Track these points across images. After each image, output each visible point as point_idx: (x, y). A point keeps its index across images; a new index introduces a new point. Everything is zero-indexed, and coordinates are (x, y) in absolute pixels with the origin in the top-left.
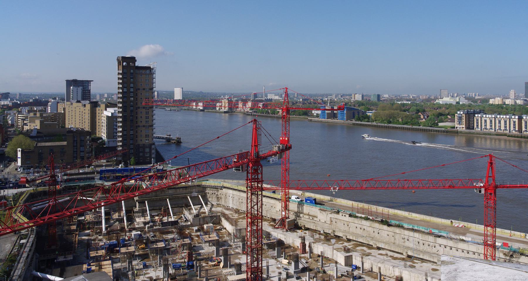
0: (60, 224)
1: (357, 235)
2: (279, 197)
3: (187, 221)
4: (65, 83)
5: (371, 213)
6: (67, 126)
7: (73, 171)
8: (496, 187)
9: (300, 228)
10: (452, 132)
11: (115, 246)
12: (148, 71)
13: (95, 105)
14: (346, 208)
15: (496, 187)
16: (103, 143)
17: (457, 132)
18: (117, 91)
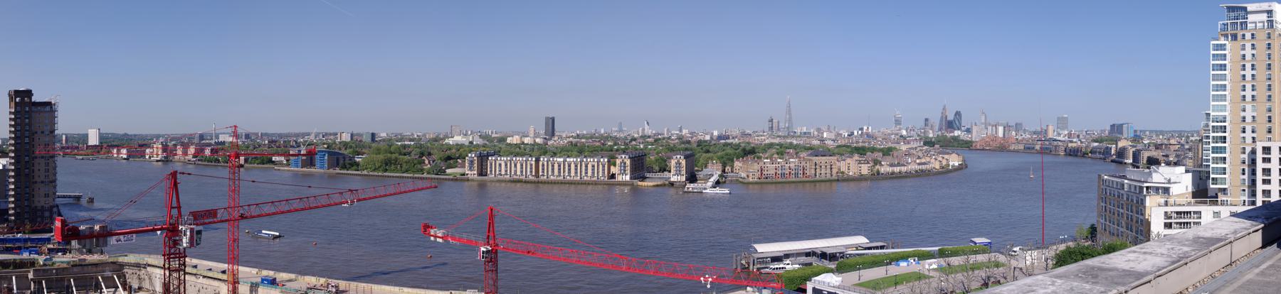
12: (48, 108)
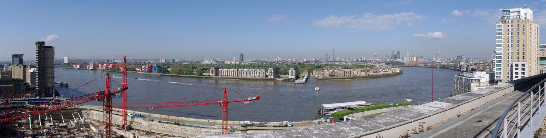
0: (11, 123)
1: (163, 131)
2: (121, 114)
3: (72, 126)
4: (11, 56)
5: (170, 120)
6: (13, 77)
7: (15, 99)
8: (228, 102)
9: (133, 129)
10: (209, 78)
11: (36, 135)
12: (51, 49)
13: (25, 67)
14: (157, 118)
15: (228, 102)
16: (29, 86)
17: (211, 78)
18: (35, 59)
